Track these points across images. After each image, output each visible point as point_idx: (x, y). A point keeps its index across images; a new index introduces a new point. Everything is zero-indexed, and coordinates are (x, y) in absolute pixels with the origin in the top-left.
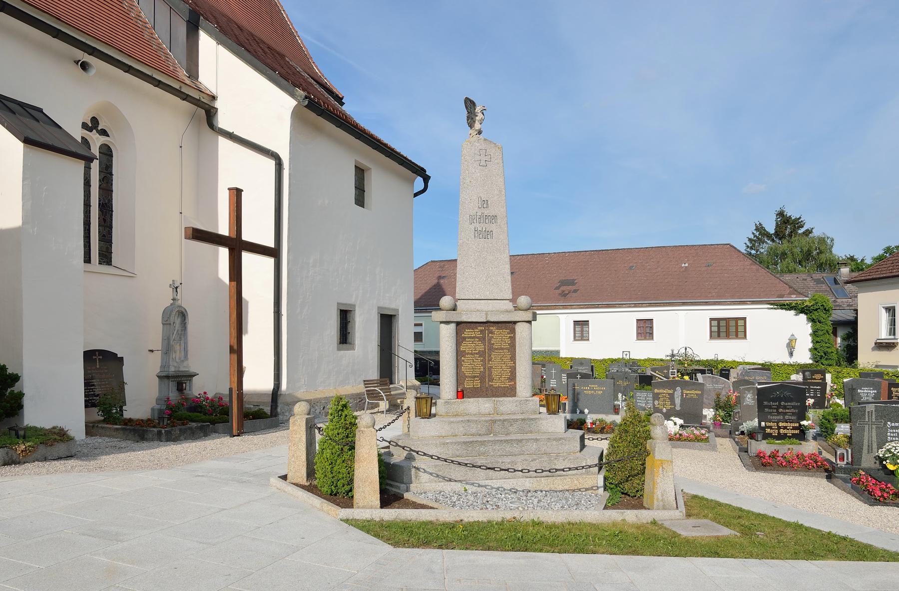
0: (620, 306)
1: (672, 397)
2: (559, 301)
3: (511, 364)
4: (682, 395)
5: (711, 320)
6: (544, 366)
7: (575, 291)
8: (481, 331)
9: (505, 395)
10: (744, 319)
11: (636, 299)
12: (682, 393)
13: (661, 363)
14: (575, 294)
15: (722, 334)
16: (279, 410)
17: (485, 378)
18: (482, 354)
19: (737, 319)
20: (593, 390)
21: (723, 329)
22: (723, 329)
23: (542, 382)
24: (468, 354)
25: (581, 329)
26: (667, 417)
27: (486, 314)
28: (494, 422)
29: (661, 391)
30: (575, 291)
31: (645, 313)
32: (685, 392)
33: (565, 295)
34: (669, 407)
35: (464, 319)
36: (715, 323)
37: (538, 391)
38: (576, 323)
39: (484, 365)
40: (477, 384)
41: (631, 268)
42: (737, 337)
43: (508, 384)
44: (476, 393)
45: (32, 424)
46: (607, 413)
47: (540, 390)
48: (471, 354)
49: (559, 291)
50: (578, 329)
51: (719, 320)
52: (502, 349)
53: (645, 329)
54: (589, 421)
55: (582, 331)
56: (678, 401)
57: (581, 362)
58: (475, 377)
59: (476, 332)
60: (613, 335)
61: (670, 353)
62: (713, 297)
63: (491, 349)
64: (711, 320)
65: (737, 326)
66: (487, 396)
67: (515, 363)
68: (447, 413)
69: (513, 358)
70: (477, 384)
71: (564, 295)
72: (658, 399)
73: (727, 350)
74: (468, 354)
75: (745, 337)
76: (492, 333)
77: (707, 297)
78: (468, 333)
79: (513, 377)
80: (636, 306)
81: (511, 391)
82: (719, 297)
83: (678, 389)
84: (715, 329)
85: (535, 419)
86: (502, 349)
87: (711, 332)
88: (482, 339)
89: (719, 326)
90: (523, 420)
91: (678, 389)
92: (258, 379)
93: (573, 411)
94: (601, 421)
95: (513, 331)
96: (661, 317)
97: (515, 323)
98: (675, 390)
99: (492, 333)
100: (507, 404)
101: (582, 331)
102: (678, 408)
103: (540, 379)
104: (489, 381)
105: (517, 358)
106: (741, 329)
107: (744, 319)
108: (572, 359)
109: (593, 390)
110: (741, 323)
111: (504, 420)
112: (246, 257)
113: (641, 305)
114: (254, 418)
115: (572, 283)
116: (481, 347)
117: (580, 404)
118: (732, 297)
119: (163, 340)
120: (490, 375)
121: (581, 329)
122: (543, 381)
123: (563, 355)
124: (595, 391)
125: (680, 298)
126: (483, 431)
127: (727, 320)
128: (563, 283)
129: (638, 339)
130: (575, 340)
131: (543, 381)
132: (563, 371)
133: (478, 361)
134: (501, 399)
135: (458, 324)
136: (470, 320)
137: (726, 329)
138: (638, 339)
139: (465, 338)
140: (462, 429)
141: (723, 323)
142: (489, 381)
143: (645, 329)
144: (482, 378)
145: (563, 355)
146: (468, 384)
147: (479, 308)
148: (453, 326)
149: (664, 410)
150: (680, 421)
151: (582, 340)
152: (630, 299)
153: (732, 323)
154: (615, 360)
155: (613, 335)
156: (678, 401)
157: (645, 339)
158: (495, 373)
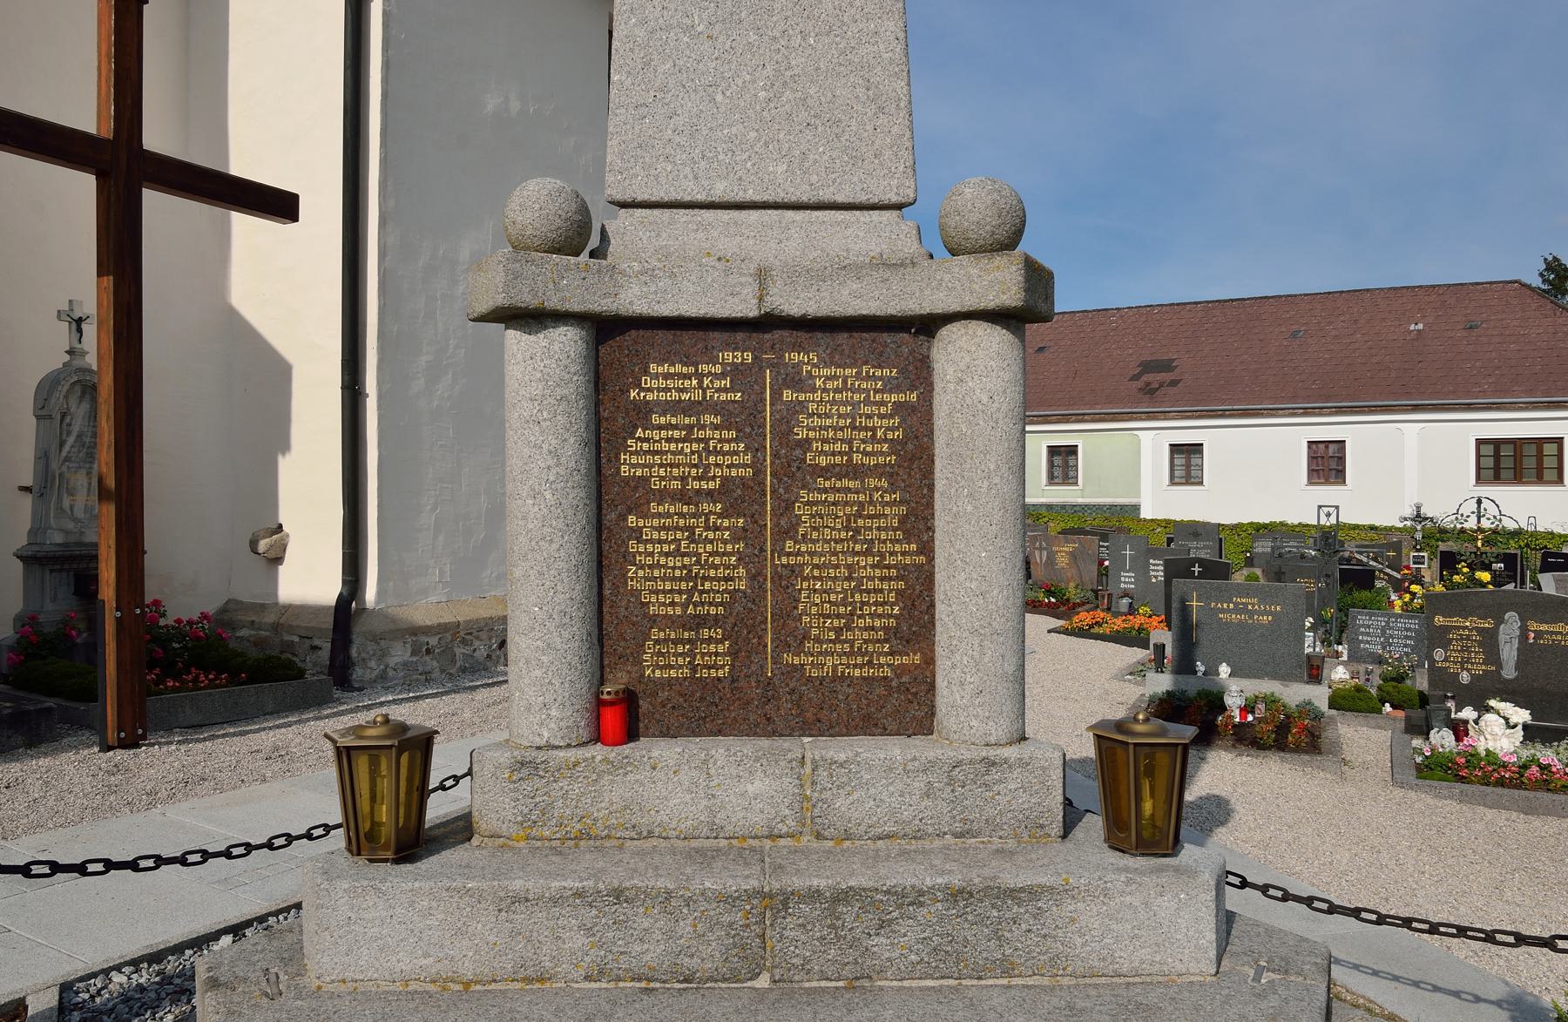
0: (1272, 413)
1: (1489, 642)
2: (1138, 403)
3: (904, 553)
4: (1524, 636)
5: (1480, 442)
6: (1104, 537)
7: (1174, 383)
8: (735, 371)
9: (868, 725)
10: (1559, 441)
11: (1308, 399)
12: (1524, 631)
13: (1372, 534)
14: (1172, 391)
15: (1503, 474)
16: (354, 653)
17: (757, 629)
18: (737, 497)
19: (1539, 442)
20: (1245, 610)
21: (1507, 463)
22: (1507, 463)
23: (1100, 575)
24: (663, 495)
25: (1186, 462)
26: (1478, 697)
27: (762, 276)
28: (778, 903)
29: (1456, 621)
30: (1174, 383)
31: (1327, 429)
32: (1534, 626)
33: (1152, 392)
34: (1479, 670)
35: (635, 299)
36: (1488, 450)
37: (1090, 595)
38: (1175, 449)
39: (752, 560)
40: (716, 658)
41: (1294, 335)
42: (1540, 479)
43: (886, 664)
44: (707, 711)
45: (1149, 517)
46: (1285, 677)
47: (1095, 592)
48: (682, 496)
49: (1140, 384)
50: (1180, 460)
51: (1497, 443)
52: (856, 472)
53: (1327, 464)
54: (1233, 701)
55: (1188, 466)
56: (1509, 653)
57: (1195, 530)
58: (700, 622)
59: (710, 378)
60: (1253, 474)
61: (1409, 512)
62: (1484, 393)
63: (794, 467)
64: (1480, 442)
65: (1540, 456)
66: (767, 727)
67: (927, 549)
68: (526, 823)
69: (918, 523)
70: (716, 658)
71: (1150, 391)
72: (1445, 644)
73: (1527, 508)
74: (663, 495)
75: (1560, 480)
76: (797, 381)
77: (1468, 394)
78: (660, 381)
79: (915, 621)
80: (1307, 412)
81: (905, 705)
82: (1496, 393)
83: (1512, 616)
84: (1490, 462)
85: (1033, 892)
86: (856, 472)
87: (1479, 468)
88: (743, 420)
89: (1497, 456)
90: (956, 895)
91: (1512, 616)
92: (309, 578)
93: (1184, 666)
94: (1271, 701)
95: (920, 375)
96: (1360, 435)
97: (928, 325)
98: (1500, 621)
99: (797, 381)
100: (874, 776)
101: (1188, 466)
102: (1509, 672)
103: (1095, 567)
104: (782, 645)
105: (940, 523)
106: (1549, 462)
107: (1559, 441)
108: (1167, 523)
109: (1245, 610)
110: (1550, 449)
111: (842, 897)
112: (161, 211)
113: (1319, 411)
114: (252, 680)
115: (1167, 366)
116: (735, 462)
117: (1204, 649)
118: (1530, 393)
119: (37, 459)
120: (787, 612)
121: (1186, 462)
122: (1103, 573)
123: (1146, 513)
124: (1251, 614)
125: (1408, 395)
126: (709, 955)
127: (1517, 443)
128: (1147, 367)
129: (1310, 482)
130: (1173, 482)
131: (1103, 573)
132: (1153, 553)
133: (719, 543)
134: (837, 749)
135: (605, 329)
136: (666, 310)
137: (1506, 462)
138: (1310, 482)
139: (642, 413)
140: (579, 941)
141: (1506, 451)
142: (782, 645)
143: (1327, 464)
144: (740, 625)
145: (1146, 513)
146: (661, 663)
147: (728, 246)
148: (565, 342)
149: (1465, 677)
150: (1521, 715)
151: (1187, 483)
152: (1294, 399)
153: (1531, 450)
154: (1265, 526)
155: (1253, 474)
156: (1509, 653)
157: (1327, 482)
158: (811, 604)
